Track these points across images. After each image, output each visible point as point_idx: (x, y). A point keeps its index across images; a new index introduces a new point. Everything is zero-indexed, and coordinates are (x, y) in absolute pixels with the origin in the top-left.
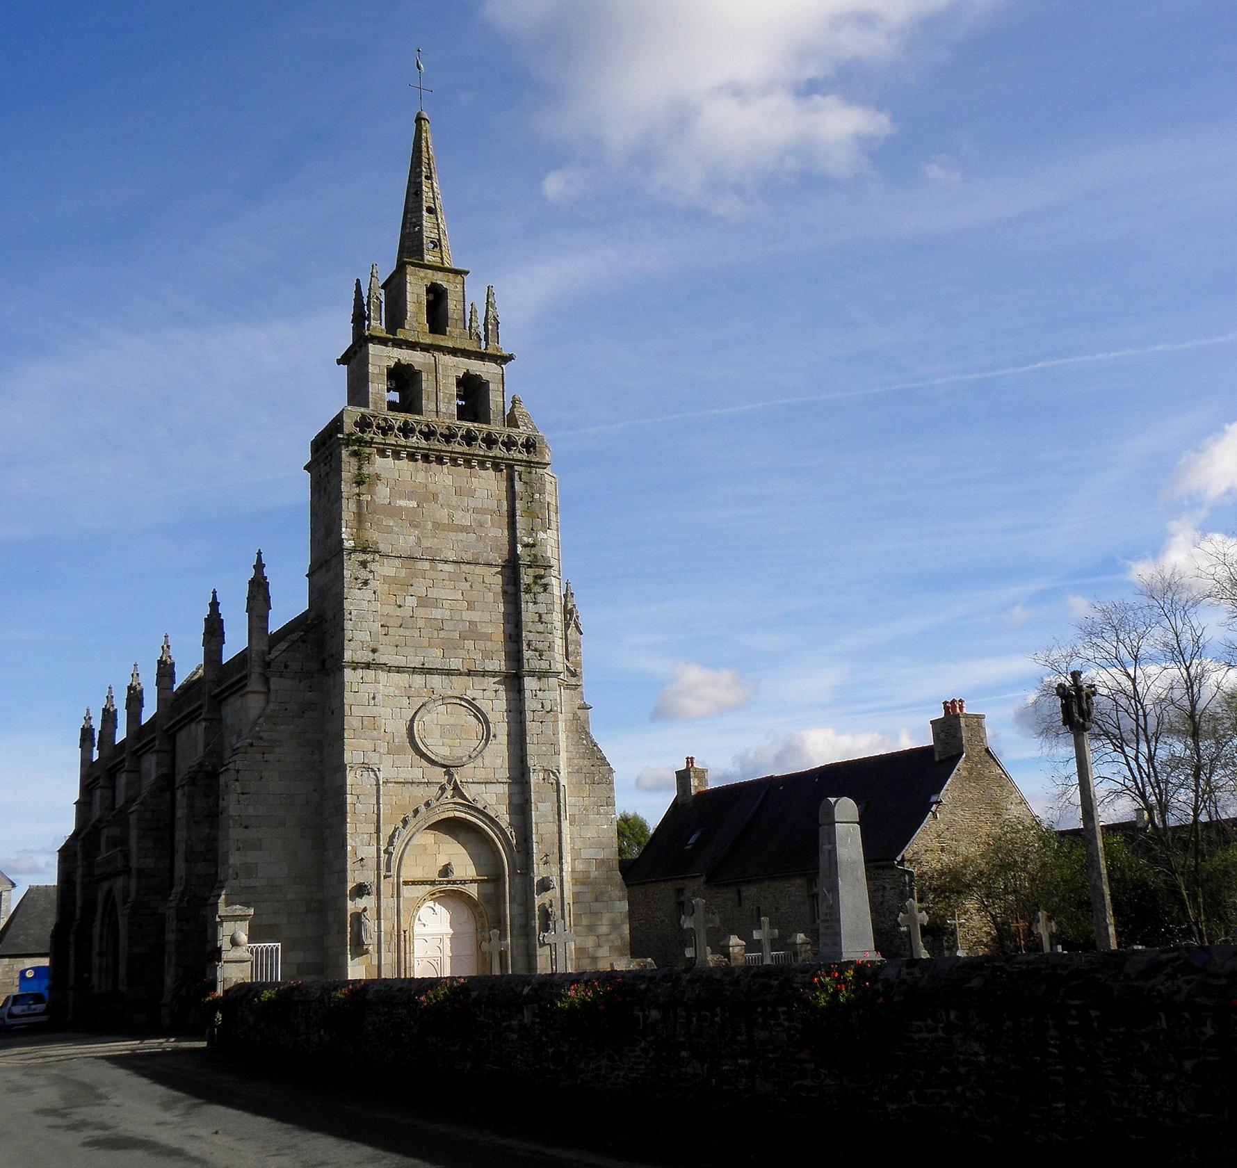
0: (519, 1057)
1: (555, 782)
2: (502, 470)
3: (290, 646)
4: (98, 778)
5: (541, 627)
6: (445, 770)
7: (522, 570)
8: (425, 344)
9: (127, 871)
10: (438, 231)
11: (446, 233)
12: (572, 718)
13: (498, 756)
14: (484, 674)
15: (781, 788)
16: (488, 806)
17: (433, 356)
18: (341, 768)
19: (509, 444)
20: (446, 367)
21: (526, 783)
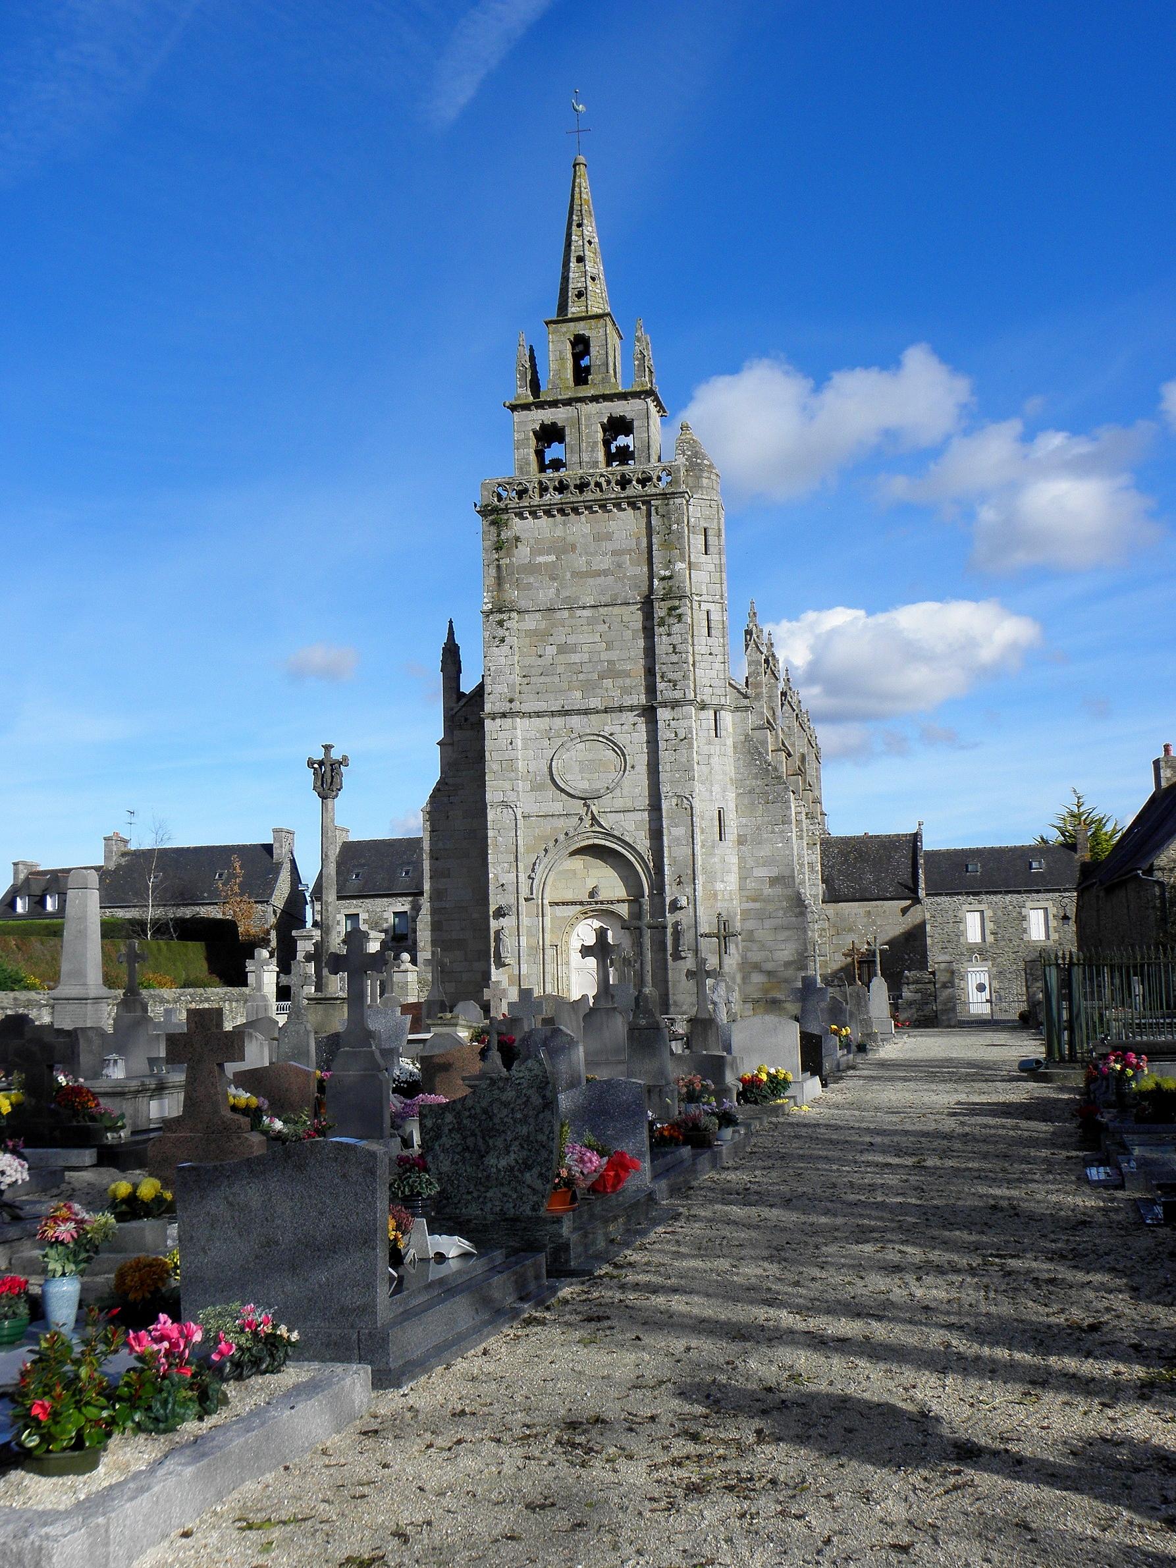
5: (674, 658)
7: (656, 605)
13: (636, 784)
14: (621, 709)
20: (588, 417)
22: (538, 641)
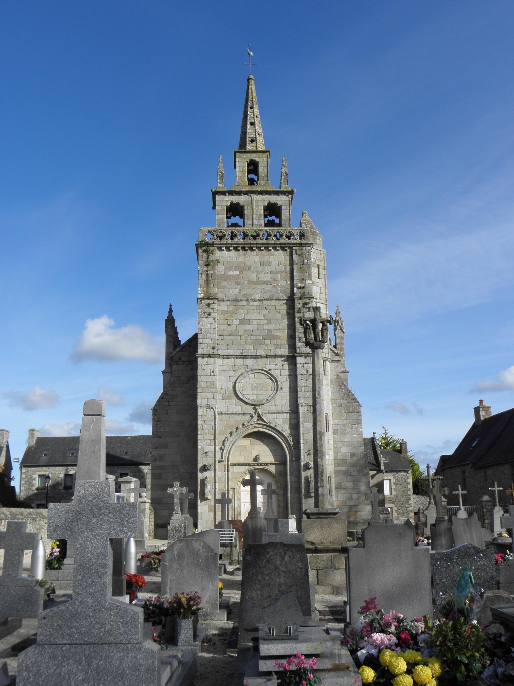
10: (255, 133)
12: (336, 378)
14: (275, 356)
16: (277, 425)
20: (257, 202)
22: (228, 317)
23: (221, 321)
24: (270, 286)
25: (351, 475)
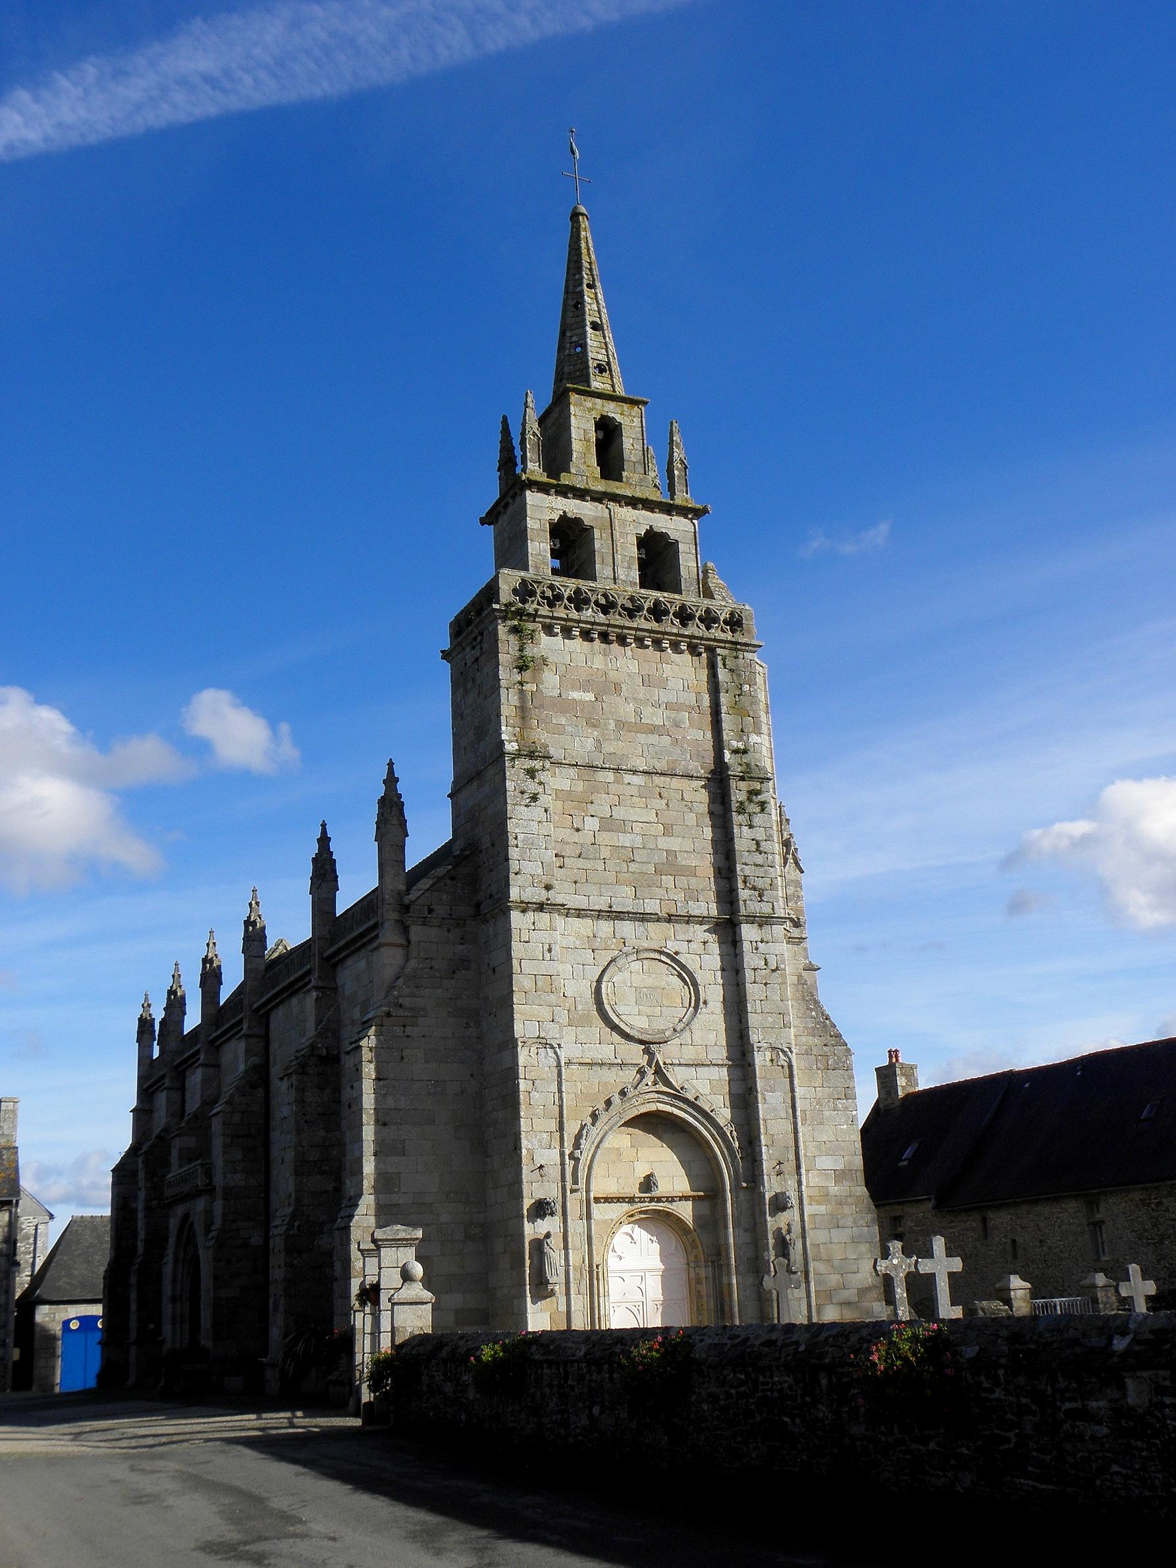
0: (1115, 1468)
1: (786, 1064)
2: (699, 654)
3: (436, 883)
4: (163, 1077)
5: (759, 859)
6: (644, 1047)
7: (733, 783)
8: (597, 492)
9: (210, 1190)
10: (607, 352)
11: (615, 355)
14: (689, 919)
15: (1027, 1085)
16: (701, 1096)
17: (607, 508)
18: (510, 1044)
19: (709, 619)
20: (623, 522)
21: (750, 1065)
23: (556, 818)
24: (666, 740)
25: (838, 1227)
